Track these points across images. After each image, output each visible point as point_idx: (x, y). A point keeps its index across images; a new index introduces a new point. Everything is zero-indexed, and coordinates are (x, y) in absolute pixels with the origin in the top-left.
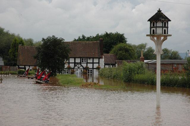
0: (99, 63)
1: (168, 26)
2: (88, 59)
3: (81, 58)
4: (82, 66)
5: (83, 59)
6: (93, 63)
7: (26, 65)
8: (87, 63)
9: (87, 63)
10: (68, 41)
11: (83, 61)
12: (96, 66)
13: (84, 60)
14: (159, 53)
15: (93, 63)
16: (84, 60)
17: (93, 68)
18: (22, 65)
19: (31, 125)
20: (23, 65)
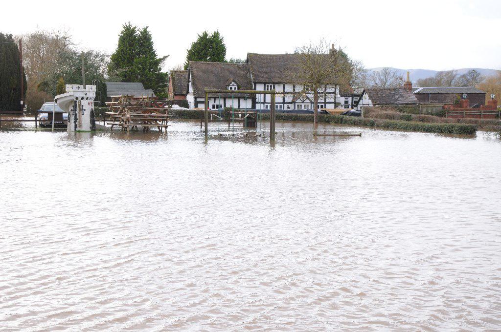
0: (335, 93)
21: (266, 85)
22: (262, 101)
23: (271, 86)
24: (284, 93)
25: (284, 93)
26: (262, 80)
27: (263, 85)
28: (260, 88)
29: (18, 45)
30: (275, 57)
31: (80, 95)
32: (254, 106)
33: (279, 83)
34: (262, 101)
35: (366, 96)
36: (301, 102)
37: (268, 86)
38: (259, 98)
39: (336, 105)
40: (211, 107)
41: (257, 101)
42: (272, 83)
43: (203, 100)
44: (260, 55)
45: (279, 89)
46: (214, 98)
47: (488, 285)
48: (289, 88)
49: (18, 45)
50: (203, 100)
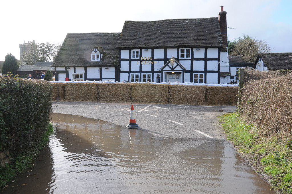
0: (218, 59)
1: (231, 71)
2: (194, 50)
3: (178, 47)
4: (181, 66)
5: (183, 51)
6: (206, 59)
7: (58, 66)
8: (193, 59)
9: (193, 59)
10: (161, 20)
11: (183, 56)
12: (212, 65)
13: (185, 53)
14: (67, 157)
15: (206, 59)
16: (185, 53)
17: (206, 71)
18: (61, 66)
19: (133, 178)
20: (63, 66)
21: (132, 51)
22: (128, 70)
23: (137, 52)
24: (153, 59)
25: (153, 59)
26: (129, 45)
27: (128, 51)
28: (125, 54)
29: (53, 174)
30: (157, 22)
31: (217, 134)
32: (117, 78)
33: (147, 48)
34: (128, 70)
35: (261, 63)
36: (170, 69)
37: (134, 52)
38: (124, 66)
39: (221, 75)
40: (71, 76)
41: (122, 69)
42: (137, 48)
43: (63, 69)
44: (137, 22)
45: (147, 54)
46: (72, 66)
47: (63, 160)
48: (159, 54)
49: (53, 174)
50: (63, 69)
